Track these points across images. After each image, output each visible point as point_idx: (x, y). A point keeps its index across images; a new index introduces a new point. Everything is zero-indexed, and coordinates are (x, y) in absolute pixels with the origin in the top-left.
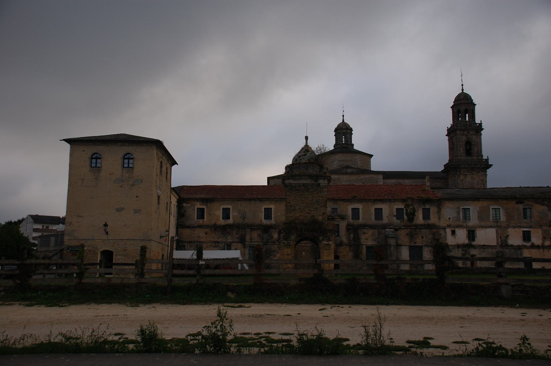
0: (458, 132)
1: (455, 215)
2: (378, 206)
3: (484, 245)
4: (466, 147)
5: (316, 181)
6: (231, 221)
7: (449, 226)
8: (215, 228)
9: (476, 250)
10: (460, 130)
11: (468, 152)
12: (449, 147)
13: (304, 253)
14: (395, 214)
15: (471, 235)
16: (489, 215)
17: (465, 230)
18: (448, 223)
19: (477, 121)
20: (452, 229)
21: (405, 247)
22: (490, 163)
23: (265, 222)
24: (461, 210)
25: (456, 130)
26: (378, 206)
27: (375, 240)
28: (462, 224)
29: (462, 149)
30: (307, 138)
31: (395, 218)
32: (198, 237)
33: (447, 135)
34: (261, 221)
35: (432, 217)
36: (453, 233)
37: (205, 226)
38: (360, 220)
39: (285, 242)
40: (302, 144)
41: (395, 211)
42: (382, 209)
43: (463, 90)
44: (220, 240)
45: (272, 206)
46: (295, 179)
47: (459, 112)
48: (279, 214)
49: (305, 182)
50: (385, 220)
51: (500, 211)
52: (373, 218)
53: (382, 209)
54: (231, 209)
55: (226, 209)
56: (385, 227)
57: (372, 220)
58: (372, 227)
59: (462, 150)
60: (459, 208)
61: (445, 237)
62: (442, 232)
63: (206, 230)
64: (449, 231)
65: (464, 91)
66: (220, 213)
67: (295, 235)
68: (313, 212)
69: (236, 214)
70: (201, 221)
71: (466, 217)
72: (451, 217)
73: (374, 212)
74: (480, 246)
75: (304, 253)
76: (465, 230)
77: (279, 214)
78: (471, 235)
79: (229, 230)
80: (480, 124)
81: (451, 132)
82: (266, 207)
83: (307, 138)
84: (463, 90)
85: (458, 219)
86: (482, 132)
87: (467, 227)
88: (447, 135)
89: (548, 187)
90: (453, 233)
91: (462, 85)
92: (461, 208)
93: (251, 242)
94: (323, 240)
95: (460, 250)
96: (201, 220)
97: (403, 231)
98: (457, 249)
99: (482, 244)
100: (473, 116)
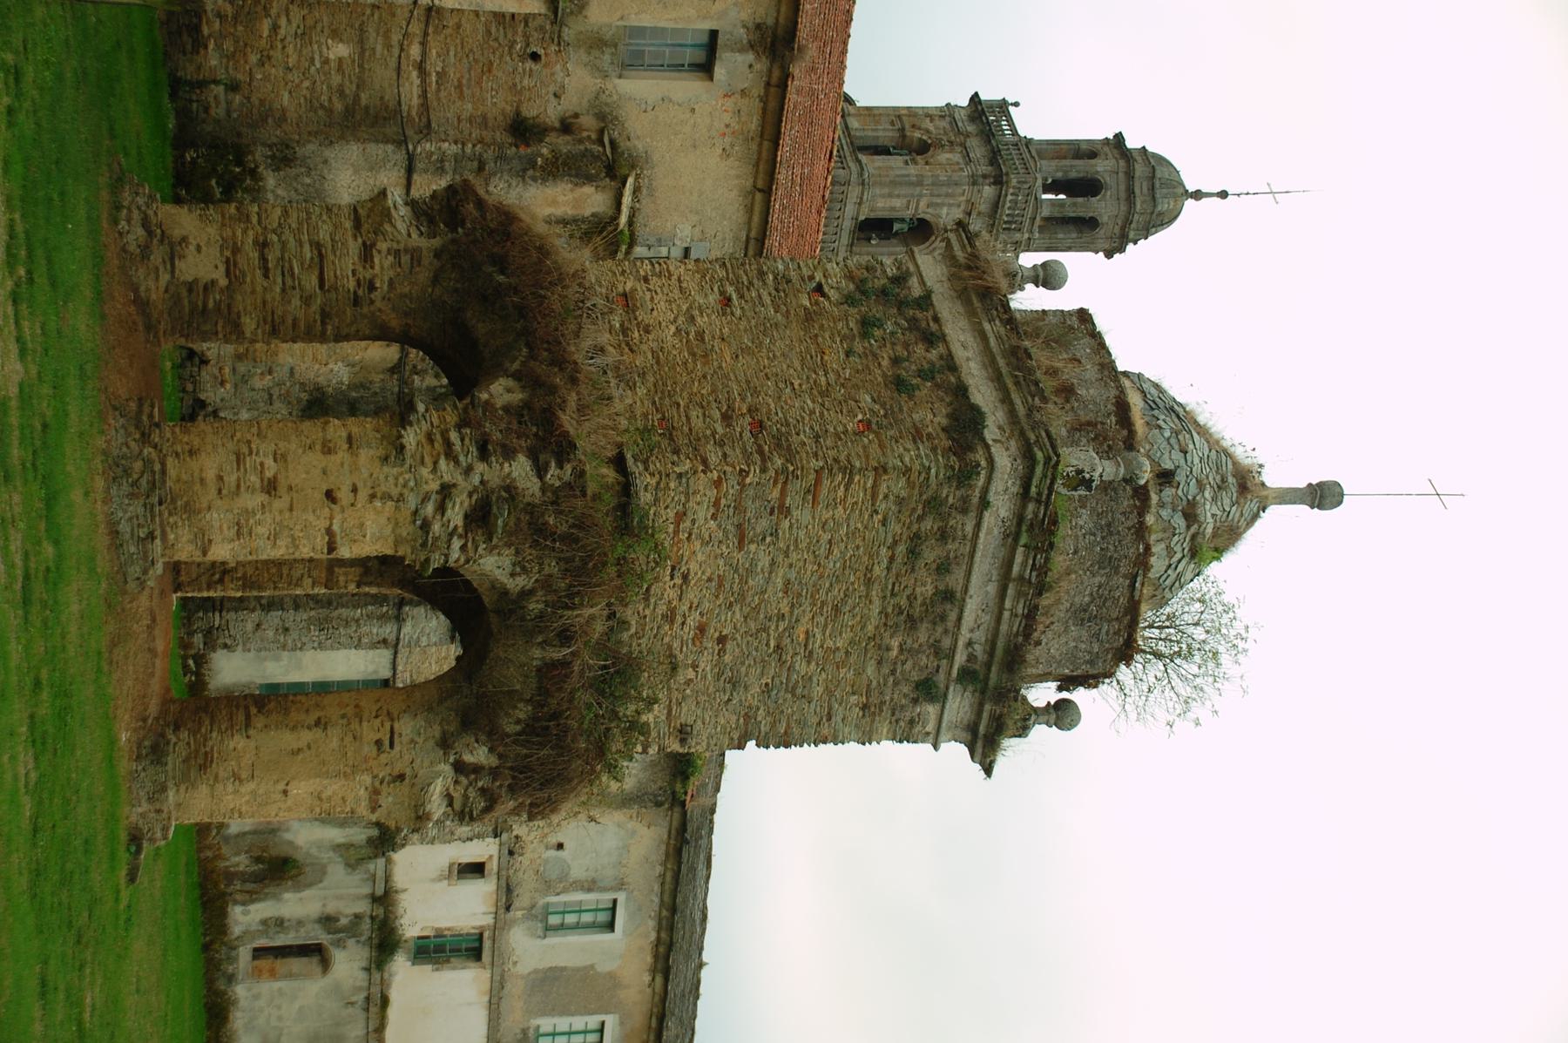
0: (988, 191)
1: (578, 872)
3: (385, 1002)
5: (967, 675)
9: (363, 975)
10: (996, 205)
12: (911, 111)
13: (340, 50)
15: (438, 950)
16: (565, 1012)
17: (488, 920)
20: (493, 866)
25: (999, 181)
29: (898, 203)
30: (1323, 496)
33: (975, 98)
43: (1198, 195)
46: (1011, 537)
49: (972, 607)
60: (620, 885)
65: (1189, 203)
67: (517, 584)
68: (705, 663)
74: (384, 985)
75: (340, 50)
78: (438, 950)
81: (986, 117)
83: (1323, 496)
84: (1198, 195)
87: (498, 927)
88: (975, 98)
92: (621, 897)
94: (459, 767)
95: (363, 907)
98: (367, 890)
99: (394, 995)
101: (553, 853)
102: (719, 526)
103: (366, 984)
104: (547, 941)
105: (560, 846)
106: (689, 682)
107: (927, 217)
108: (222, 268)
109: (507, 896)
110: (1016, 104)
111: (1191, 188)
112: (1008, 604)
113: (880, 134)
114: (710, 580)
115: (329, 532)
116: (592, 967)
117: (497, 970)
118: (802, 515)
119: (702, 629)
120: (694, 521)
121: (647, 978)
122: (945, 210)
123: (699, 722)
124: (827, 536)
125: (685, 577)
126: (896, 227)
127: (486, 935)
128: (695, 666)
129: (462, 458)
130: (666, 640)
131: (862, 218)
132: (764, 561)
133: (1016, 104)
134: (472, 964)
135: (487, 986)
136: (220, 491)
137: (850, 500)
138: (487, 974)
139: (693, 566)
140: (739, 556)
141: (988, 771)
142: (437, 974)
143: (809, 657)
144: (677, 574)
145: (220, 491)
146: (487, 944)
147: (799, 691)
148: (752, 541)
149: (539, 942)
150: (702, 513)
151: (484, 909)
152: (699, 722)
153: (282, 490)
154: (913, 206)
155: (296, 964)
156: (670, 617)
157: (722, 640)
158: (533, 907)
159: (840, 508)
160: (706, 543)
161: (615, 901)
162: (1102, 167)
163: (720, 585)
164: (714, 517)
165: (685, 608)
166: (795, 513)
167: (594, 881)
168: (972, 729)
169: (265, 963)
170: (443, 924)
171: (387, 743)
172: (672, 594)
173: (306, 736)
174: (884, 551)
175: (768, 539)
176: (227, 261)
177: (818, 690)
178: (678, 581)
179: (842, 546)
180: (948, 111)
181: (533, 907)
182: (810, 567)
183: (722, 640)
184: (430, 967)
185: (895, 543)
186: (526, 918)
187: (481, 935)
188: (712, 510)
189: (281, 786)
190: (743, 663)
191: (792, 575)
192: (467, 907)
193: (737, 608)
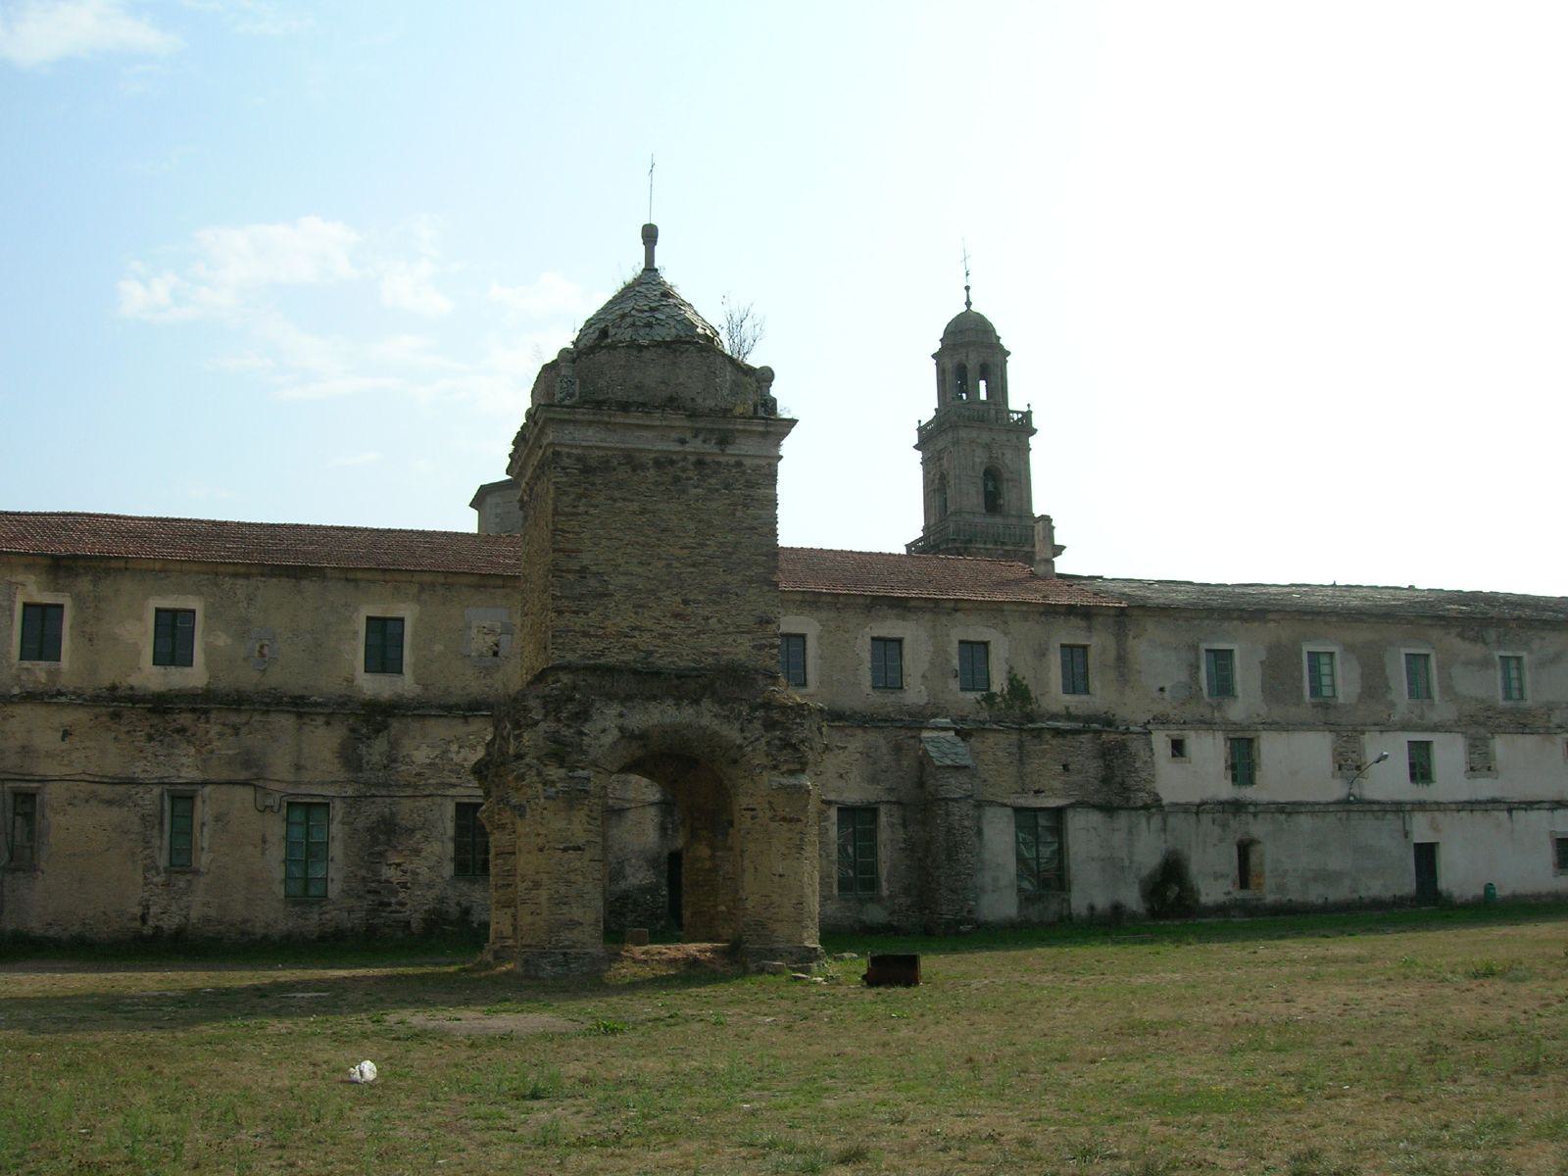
1: (1183, 676)
2: (889, 628)
4: (986, 485)
6: (194, 676)
7: (1162, 721)
8: (118, 704)
11: (993, 502)
14: (956, 662)
15: (1243, 763)
18: (1158, 709)
19: (1016, 402)
20: (1175, 733)
21: (1000, 811)
22: (1057, 542)
23: (373, 686)
24: (1203, 656)
26: (889, 628)
27: (873, 780)
28: (1207, 713)
30: (650, 235)
31: (954, 685)
32: (25, 750)
33: (917, 447)
34: (350, 681)
35: (1095, 683)
36: (1178, 748)
37: (60, 693)
38: (812, 688)
39: (555, 772)
40: (631, 266)
41: (954, 649)
42: (899, 641)
43: (968, 303)
44: (137, 770)
45: (407, 611)
47: (961, 372)
48: (438, 648)
50: (915, 693)
51: (1331, 664)
52: (866, 679)
53: (899, 641)
54: (199, 617)
55: (174, 612)
56: (916, 720)
57: (862, 693)
58: (865, 721)
59: (972, 498)
60: (1194, 648)
61: (1150, 763)
62: (1136, 745)
63: (68, 717)
64: (1161, 741)
65: (973, 308)
66: (141, 634)
69: (222, 640)
70: (40, 670)
71: (1223, 687)
72: (1168, 686)
73: (866, 656)
76: (1220, 737)
77: (438, 648)
78: (1243, 763)
79: (185, 719)
80: (1027, 415)
82: (376, 612)
83: (650, 235)
84: (968, 303)
85: (1194, 694)
86: (1032, 440)
87: (1227, 726)
88: (917, 447)
89: (1411, 587)
90: (1178, 748)
91: (967, 288)
92: (1204, 646)
93: (297, 783)
96: (44, 664)
97: (991, 739)
100: (999, 390)
101: (1167, 695)
102: (593, 610)
103: (1269, 816)
104: (1240, 695)
105: (1162, 689)
106: (720, 621)
107: (983, 470)
108: (506, 910)
109: (1206, 724)
110: (920, 422)
111: (964, 308)
112: (658, 423)
113: (937, 504)
114: (636, 613)
115: (565, 850)
116: (1262, 663)
117: (1260, 727)
118: (586, 559)
119: (676, 616)
120: (589, 626)
121: (1272, 625)
122: (977, 460)
123: (754, 613)
124: (604, 542)
125: (633, 629)
126: (990, 488)
127: (1231, 736)
128: (707, 619)
129: (522, 770)
130: (684, 637)
131: (984, 511)
132: (623, 580)
133: (920, 422)
134: (1256, 745)
135: (1274, 734)
136: (538, 914)
137: (577, 529)
138: (1264, 735)
139: (624, 624)
140: (618, 597)
141: (793, 422)
142: (1263, 767)
143: (703, 545)
144: (631, 634)
145: (538, 914)
146: (1239, 735)
147: (730, 550)
148: (607, 588)
149: (1240, 699)
150: (581, 620)
151: (1210, 739)
152: (754, 613)
153: (537, 878)
154: (975, 480)
155: (1253, 859)
156: (666, 637)
157: (686, 602)
158: (1211, 706)
159: (582, 535)
160: (607, 618)
161: (1207, 650)
162: (949, 365)
163: (640, 606)
164: (586, 614)
165: (658, 627)
166: (585, 563)
167: (1191, 665)
168: (764, 435)
169: (1253, 881)
170: (1222, 764)
171: (752, 813)
172: (646, 636)
173: (747, 862)
174: (618, 505)
175: (606, 578)
176: (503, 907)
177: (730, 537)
178: (636, 633)
179: (612, 532)
180: (925, 462)
181: (1211, 706)
182: (628, 551)
183: (686, 602)
184: (1257, 773)
185: (611, 498)
186: (1219, 707)
187: (1231, 739)
188: (582, 615)
189: (776, 879)
190: (706, 588)
191: (635, 561)
192: (1209, 751)
193: (660, 594)
